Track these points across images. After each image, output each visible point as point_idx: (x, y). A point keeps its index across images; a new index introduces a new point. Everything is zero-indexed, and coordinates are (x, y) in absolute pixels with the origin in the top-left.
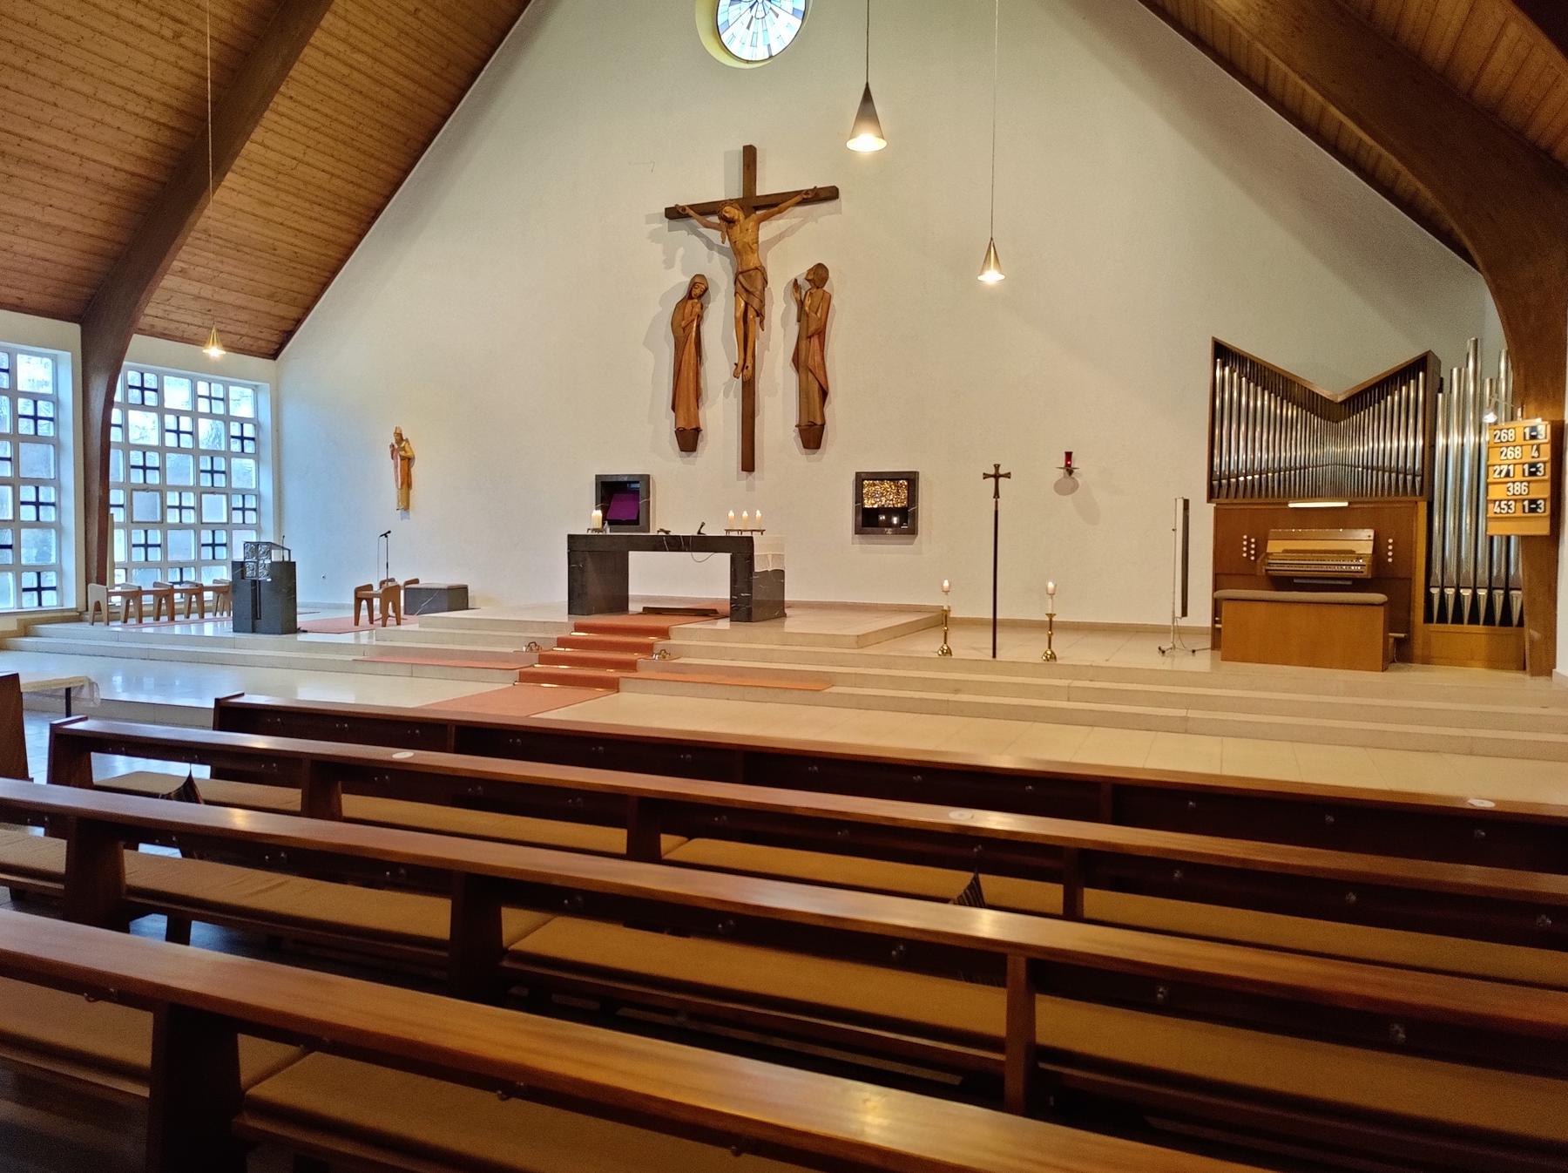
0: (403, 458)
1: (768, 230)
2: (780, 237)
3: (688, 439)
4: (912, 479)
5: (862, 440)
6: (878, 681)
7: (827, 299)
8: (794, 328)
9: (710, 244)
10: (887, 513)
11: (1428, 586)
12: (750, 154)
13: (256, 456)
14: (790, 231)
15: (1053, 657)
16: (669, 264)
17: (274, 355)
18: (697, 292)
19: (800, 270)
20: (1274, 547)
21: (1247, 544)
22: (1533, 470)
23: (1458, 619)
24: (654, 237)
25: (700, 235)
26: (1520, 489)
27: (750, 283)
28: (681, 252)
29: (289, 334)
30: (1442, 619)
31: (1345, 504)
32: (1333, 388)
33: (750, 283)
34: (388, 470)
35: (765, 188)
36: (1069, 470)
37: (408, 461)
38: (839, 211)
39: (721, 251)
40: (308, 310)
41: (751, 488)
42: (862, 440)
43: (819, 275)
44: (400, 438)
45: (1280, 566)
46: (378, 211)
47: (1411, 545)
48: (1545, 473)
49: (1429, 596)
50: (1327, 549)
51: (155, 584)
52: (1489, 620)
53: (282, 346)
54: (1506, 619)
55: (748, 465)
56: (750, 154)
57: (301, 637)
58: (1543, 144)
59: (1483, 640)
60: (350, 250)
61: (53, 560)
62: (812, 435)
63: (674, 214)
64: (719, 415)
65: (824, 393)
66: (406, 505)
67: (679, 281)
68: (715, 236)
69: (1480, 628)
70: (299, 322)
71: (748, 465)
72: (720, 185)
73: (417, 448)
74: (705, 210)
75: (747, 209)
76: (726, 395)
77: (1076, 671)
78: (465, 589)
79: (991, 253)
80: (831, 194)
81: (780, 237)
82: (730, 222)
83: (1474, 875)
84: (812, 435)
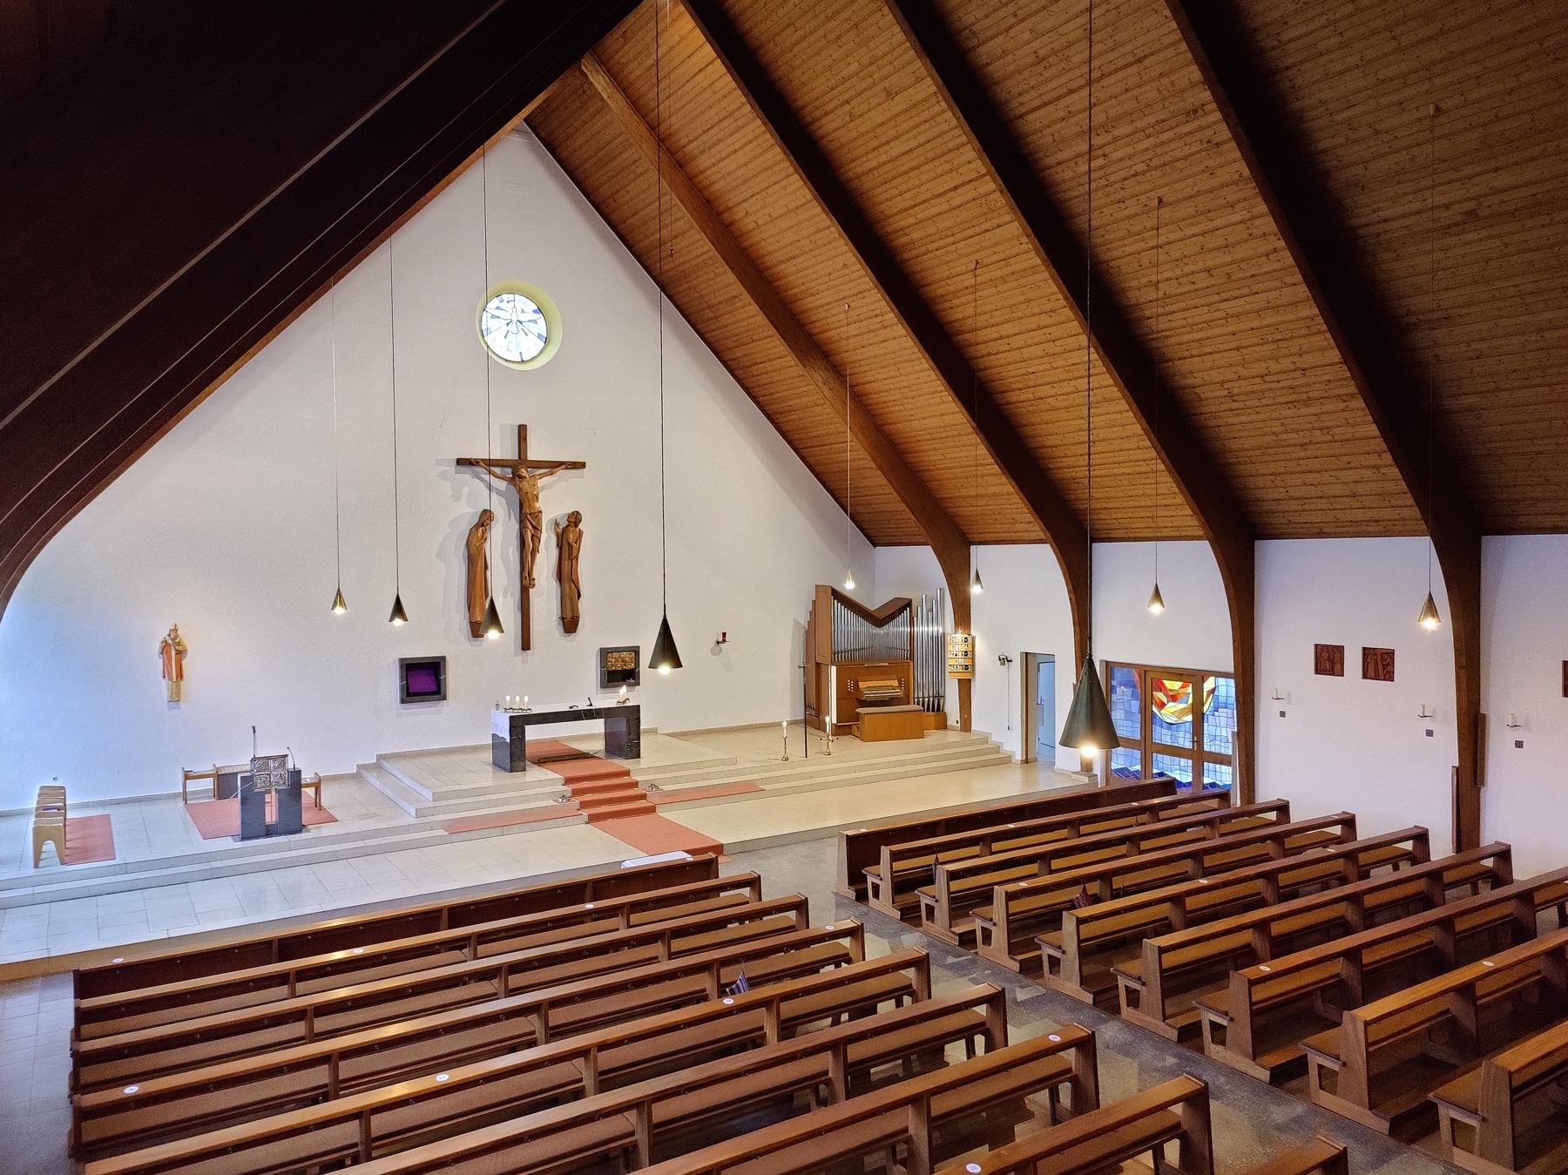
0: (179, 653)
2: (544, 487)
5: (598, 632)
8: (554, 552)
12: (522, 431)
16: (457, 497)
18: (486, 518)
24: (442, 476)
25: (482, 480)
26: (962, 661)
27: (527, 518)
28: (466, 490)
31: (834, 669)
32: (874, 603)
33: (527, 518)
35: (532, 455)
37: (180, 653)
39: (499, 492)
41: (525, 661)
42: (598, 632)
43: (575, 519)
50: (866, 682)
55: (526, 645)
56: (522, 431)
62: (570, 624)
63: (461, 462)
66: (176, 698)
67: (467, 513)
68: (502, 485)
71: (526, 645)
72: (504, 449)
74: (489, 463)
75: (518, 470)
78: (1390, 654)
81: (544, 487)
82: (521, 477)
83: (443, 1078)
84: (570, 624)
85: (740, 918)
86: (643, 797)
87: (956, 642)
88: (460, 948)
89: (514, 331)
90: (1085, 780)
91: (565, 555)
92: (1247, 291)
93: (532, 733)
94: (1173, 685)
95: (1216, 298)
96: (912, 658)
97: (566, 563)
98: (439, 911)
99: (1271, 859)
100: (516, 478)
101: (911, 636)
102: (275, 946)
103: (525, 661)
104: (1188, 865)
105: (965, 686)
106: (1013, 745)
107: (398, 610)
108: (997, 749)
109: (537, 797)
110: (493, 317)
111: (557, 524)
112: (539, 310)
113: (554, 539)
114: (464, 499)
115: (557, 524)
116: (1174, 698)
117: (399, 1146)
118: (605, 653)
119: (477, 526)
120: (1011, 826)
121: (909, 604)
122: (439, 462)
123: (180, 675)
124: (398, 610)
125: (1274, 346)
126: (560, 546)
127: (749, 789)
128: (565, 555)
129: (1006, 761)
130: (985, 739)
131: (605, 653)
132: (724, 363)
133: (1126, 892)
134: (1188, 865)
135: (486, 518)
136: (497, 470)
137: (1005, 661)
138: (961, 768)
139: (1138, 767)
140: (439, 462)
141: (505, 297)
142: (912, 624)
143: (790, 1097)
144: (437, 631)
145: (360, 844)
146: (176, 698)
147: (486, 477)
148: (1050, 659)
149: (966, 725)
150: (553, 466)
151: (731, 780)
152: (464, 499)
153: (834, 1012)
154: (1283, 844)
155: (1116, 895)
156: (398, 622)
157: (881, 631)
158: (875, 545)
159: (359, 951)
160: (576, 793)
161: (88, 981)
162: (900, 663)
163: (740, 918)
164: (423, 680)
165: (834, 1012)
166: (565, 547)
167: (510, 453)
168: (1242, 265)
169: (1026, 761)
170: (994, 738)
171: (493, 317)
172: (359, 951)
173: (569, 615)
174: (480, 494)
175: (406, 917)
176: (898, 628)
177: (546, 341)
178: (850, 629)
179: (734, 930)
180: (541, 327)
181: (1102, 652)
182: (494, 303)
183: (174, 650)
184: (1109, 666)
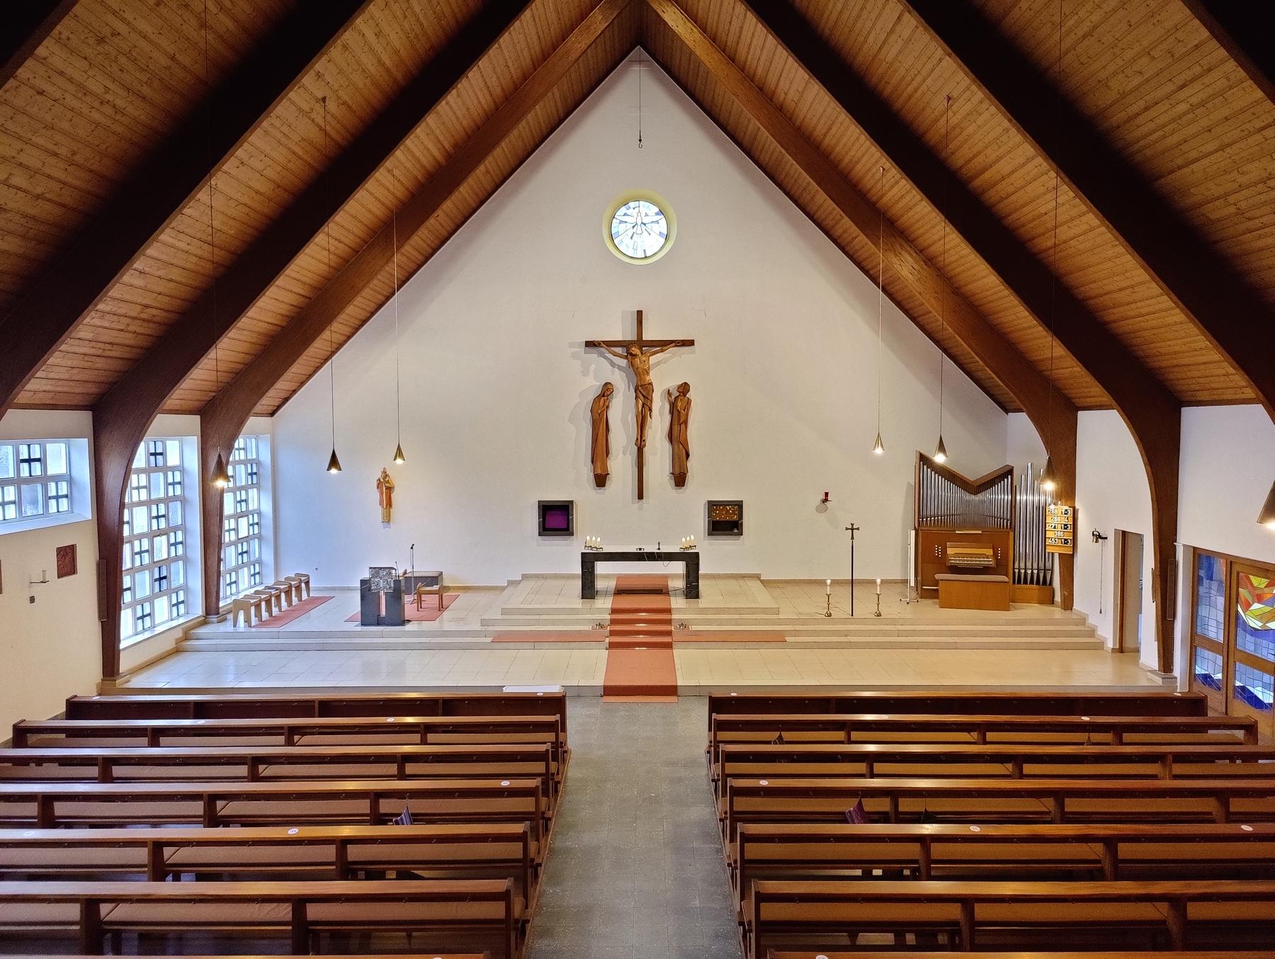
0: (387, 488)
1: (653, 359)
2: (658, 363)
3: (601, 480)
4: (739, 505)
6: (808, 633)
7: (689, 402)
8: (668, 418)
9: (613, 364)
10: (725, 521)
13: (258, 486)
14: (665, 361)
15: (879, 615)
16: (585, 373)
17: (272, 414)
18: (606, 391)
19: (673, 383)
20: (950, 551)
21: (937, 550)
22: (1066, 526)
23: (1025, 582)
24: (574, 356)
25: (606, 358)
27: (643, 392)
29: (286, 400)
30: (1019, 582)
33: (643, 392)
34: (375, 495)
35: (647, 336)
36: (826, 500)
37: (390, 489)
38: (694, 352)
39: (620, 368)
40: (303, 384)
41: (641, 509)
43: (684, 388)
44: (385, 475)
45: (954, 561)
46: (364, 322)
48: (1070, 529)
50: (973, 549)
51: (484, 622)
52: (1038, 583)
53: (279, 407)
54: (1045, 582)
57: (408, 627)
58: (874, 199)
60: (341, 345)
61: (182, 581)
62: (680, 479)
63: (590, 344)
64: (620, 464)
65: (688, 455)
66: (387, 519)
67: (592, 386)
68: (623, 362)
69: (1035, 586)
70: (294, 392)
72: (621, 331)
73: (396, 480)
74: (610, 344)
75: (635, 349)
76: (624, 454)
77: (893, 621)
79: (879, 441)
80: (690, 343)
81: (658, 363)
82: (634, 356)
83: (293, 832)
84: (680, 479)
85: (1231, 757)
86: (669, 633)
87: (1057, 515)
88: (969, 731)
89: (641, 232)
90: (1158, 681)
91: (676, 422)
92: (1197, 70)
93: (601, 568)
94: (1259, 582)
95: (1170, 87)
96: (1013, 528)
97: (676, 428)
98: (313, 701)
99: (1213, 821)
100: (630, 356)
101: (1013, 504)
102: (192, 706)
103: (641, 509)
104: (848, 806)
105: (1068, 562)
106: (1107, 632)
107: (334, 462)
108: (1092, 632)
109: (578, 622)
110: (621, 222)
111: (669, 393)
112: (661, 212)
113: (667, 406)
114: (592, 374)
115: (669, 393)
116: (1259, 599)
117: (452, 873)
118: (713, 506)
119: (599, 397)
120: (1086, 719)
121: (1009, 472)
122: (571, 345)
123: (389, 504)
124: (334, 462)
125: (1258, 138)
126: (672, 412)
127: (776, 639)
128: (676, 422)
129: (1099, 646)
130: (1083, 620)
131: (713, 506)
132: (835, 241)
133: (374, 871)
134: (1209, 805)
135: (606, 391)
136: (619, 350)
137: (1098, 537)
138: (1063, 647)
139: (1219, 676)
140: (571, 345)
141: (632, 204)
142: (1013, 492)
143: (366, 936)
144: (568, 483)
145: (428, 640)
146: (387, 519)
147: (610, 356)
148: (1140, 537)
149: (1068, 604)
150: (663, 345)
151: (532, 628)
152: (592, 374)
153: (866, 866)
154: (1227, 806)
155: (1066, 818)
156: (334, 471)
157: (980, 497)
158: (1007, 411)
159: (201, 722)
160: (613, 622)
161: (718, 704)
162: (1001, 532)
163: (1231, 757)
164: (556, 519)
165: (866, 866)
166: (676, 413)
167: (630, 336)
168: (1180, 35)
169: (1121, 649)
170: (1092, 621)
171: (621, 222)
172: (201, 722)
173: (677, 472)
174: (612, 371)
175: (378, 701)
176: (998, 496)
177: (667, 238)
179: (1222, 766)
180: (663, 222)
181: (1189, 535)
182: (623, 210)
183: (386, 487)
184: (1201, 558)
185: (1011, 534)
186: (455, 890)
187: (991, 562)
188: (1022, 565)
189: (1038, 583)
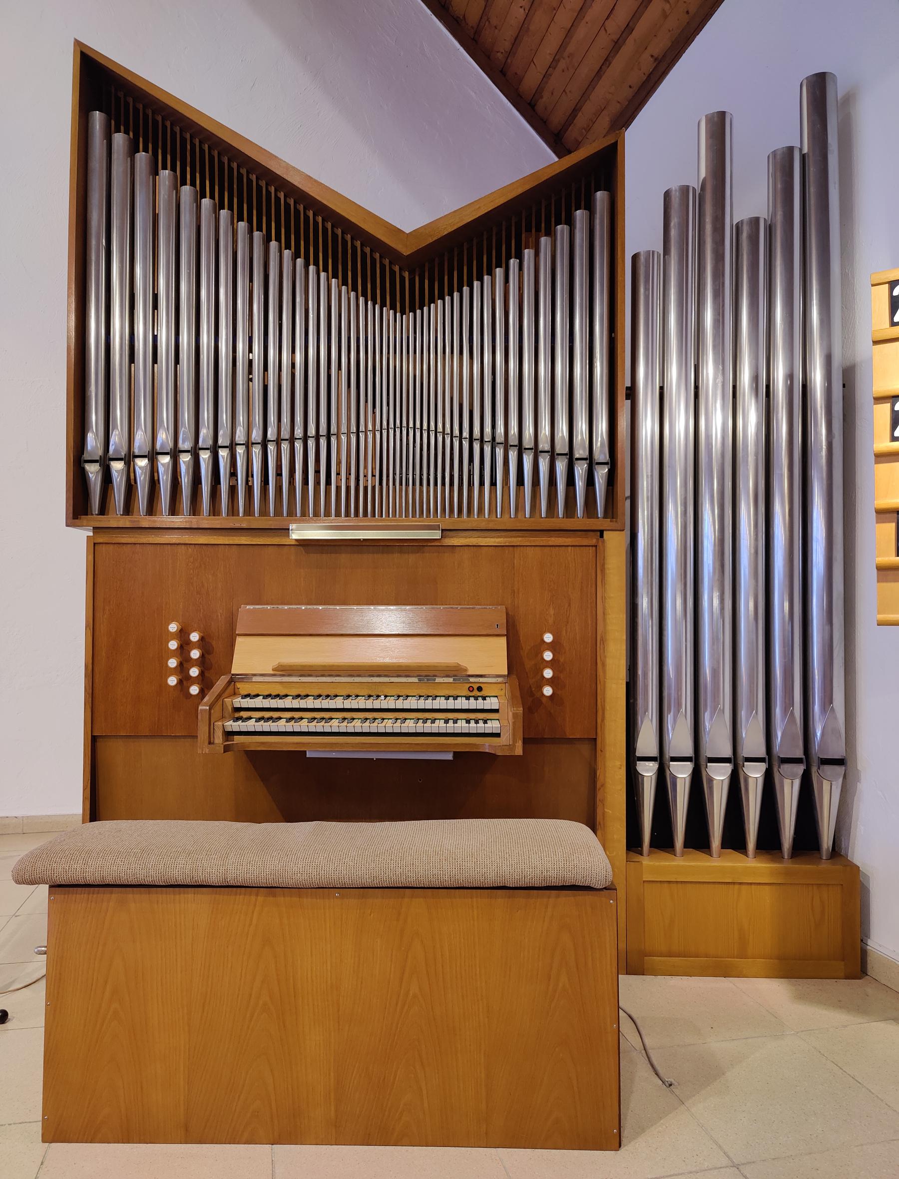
11: (632, 758)
23: (698, 839)
30: (663, 840)
47: (594, 644)
49: (633, 781)
52: (769, 842)
59: (766, 898)
69: (751, 865)
178: (228, 337)
185: (616, 542)
186: (784, 342)
187: (498, 725)
188: (680, 740)
189: (769, 842)
